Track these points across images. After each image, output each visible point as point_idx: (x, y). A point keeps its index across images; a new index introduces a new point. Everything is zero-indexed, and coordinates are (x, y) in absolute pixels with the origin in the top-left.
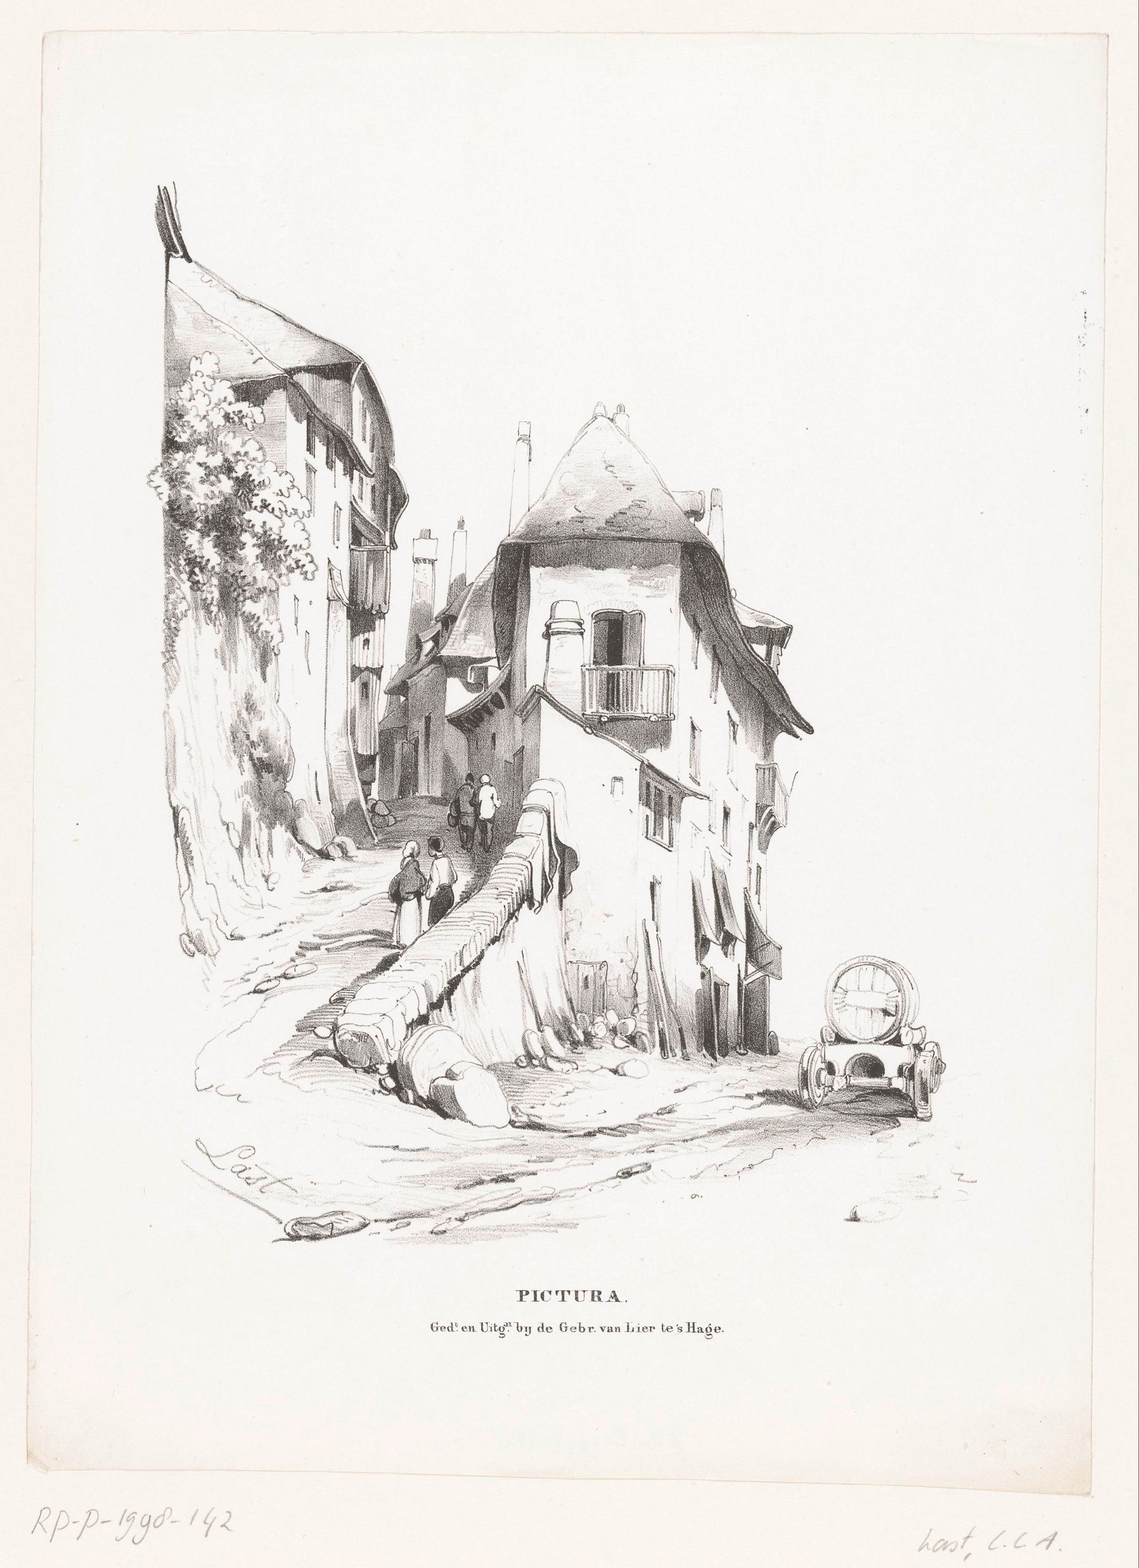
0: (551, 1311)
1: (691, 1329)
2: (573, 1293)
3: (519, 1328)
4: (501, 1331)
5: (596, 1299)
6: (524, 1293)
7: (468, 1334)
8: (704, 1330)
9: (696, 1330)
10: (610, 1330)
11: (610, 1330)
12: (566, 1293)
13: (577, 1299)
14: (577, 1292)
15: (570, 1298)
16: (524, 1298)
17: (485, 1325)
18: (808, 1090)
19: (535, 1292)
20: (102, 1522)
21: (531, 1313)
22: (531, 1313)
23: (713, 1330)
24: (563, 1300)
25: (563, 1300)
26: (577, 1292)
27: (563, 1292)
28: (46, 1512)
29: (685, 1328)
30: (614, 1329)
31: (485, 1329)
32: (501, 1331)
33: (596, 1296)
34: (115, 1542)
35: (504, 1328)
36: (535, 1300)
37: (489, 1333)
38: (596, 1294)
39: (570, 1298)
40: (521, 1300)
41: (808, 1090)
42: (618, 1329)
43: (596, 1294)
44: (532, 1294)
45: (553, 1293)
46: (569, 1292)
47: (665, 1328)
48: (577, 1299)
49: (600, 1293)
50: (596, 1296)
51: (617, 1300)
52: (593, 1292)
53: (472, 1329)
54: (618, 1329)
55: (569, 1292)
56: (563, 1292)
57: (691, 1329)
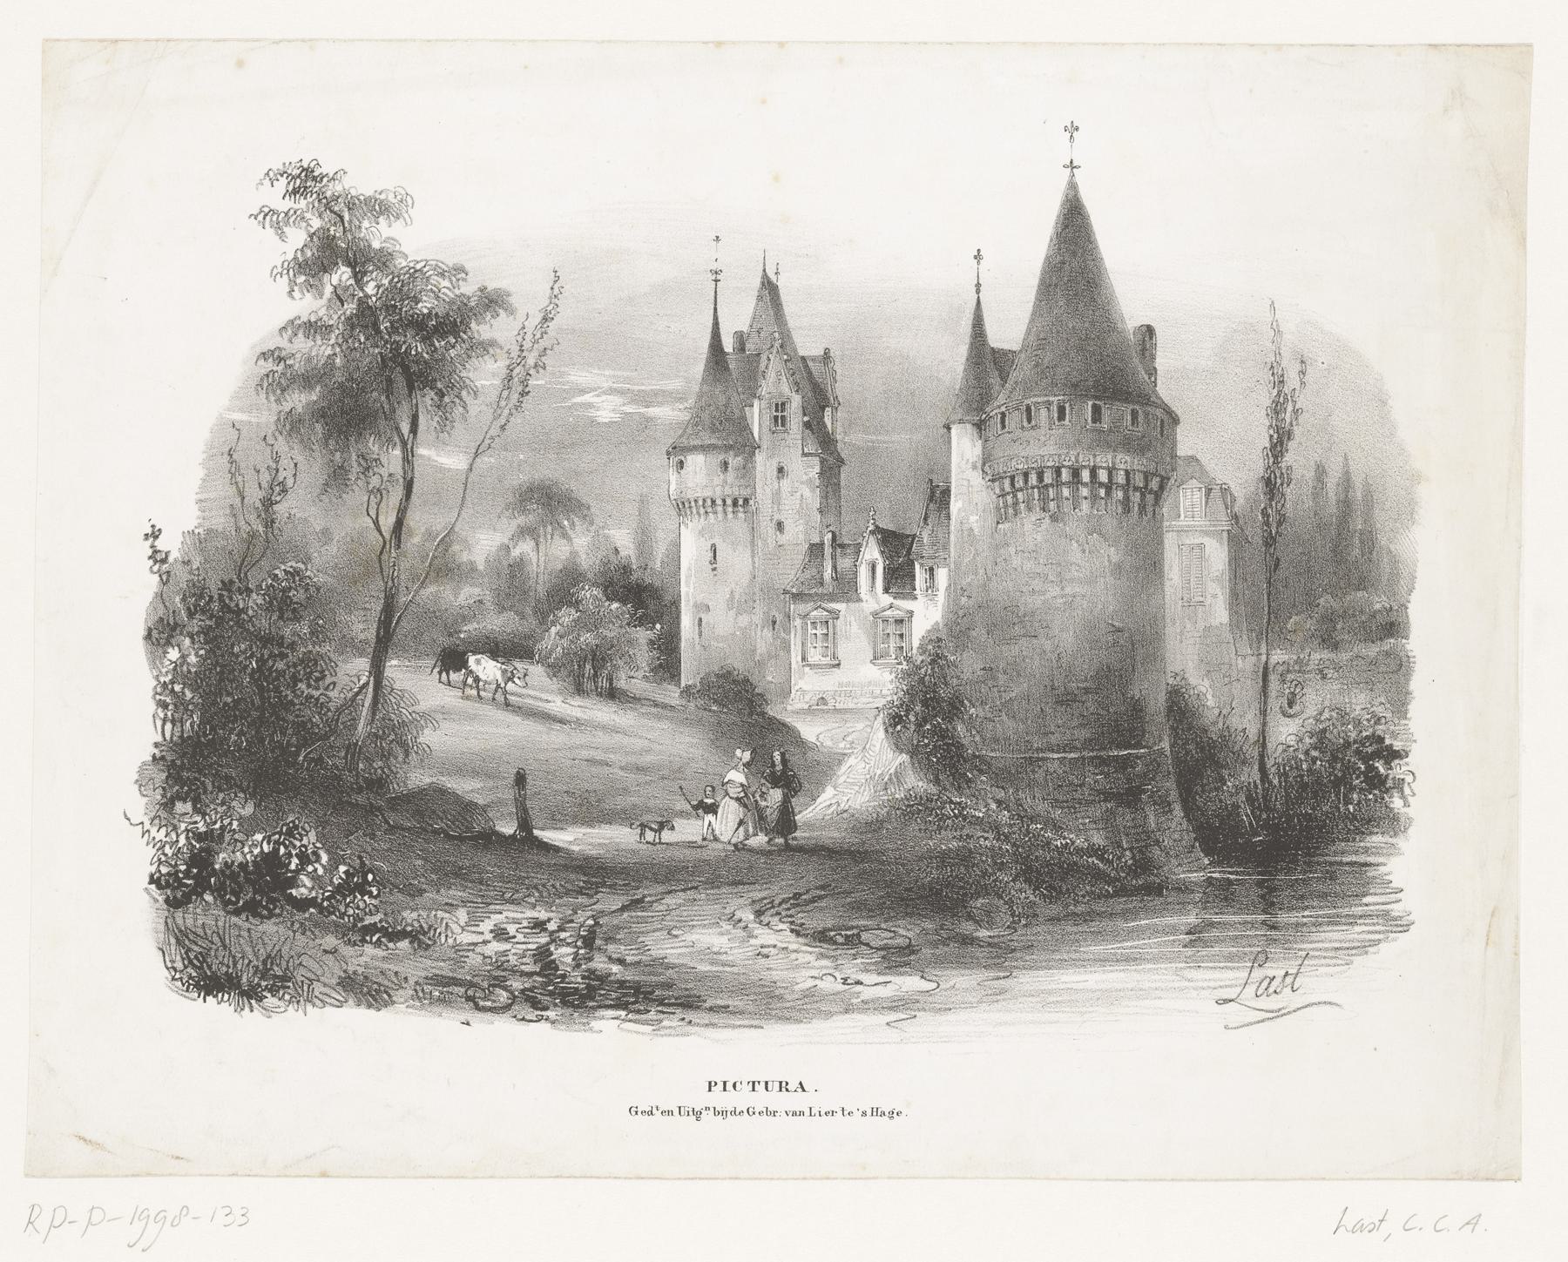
0: (742, 1099)
1: (875, 1114)
2: (763, 1084)
3: (717, 1113)
4: (698, 1115)
5: (784, 1089)
6: (713, 1084)
7: (666, 1118)
8: (887, 1113)
9: (879, 1114)
10: (794, 1114)
11: (794, 1114)
12: (756, 1083)
13: (767, 1089)
14: (767, 1083)
15: (760, 1088)
16: (713, 1089)
17: (682, 1109)
18: (623, 909)
19: (725, 1083)
20: (70, 1223)
21: (719, 1099)
22: (719, 1099)
23: (895, 1114)
24: (754, 1090)
25: (754, 1090)
26: (767, 1083)
27: (754, 1083)
28: (37, 1210)
29: (869, 1113)
30: (798, 1113)
31: (770, 1089)
32: (698, 1115)
33: (783, 1086)
34: (128, 1248)
35: (701, 1113)
36: (725, 1090)
37: (685, 1118)
38: (784, 1084)
39: (760, 1088)
40: (710, 1090)
41: (623, 909)
42: (802, 1113)
43: (784, 1084)
44: (720, 1085)
45: (745, 1083)
46: (759, 1082)
47: (846, 1113)
48: (767, 1089)
49: (787, 1084)
50: (783, 1086)
51: (804, 1090)
52: (781, 1083)
53: (670, 1113)
54: (802, 1113)
55: (759, 1082)
56: (754, 1083)
57: (875, 1114)
